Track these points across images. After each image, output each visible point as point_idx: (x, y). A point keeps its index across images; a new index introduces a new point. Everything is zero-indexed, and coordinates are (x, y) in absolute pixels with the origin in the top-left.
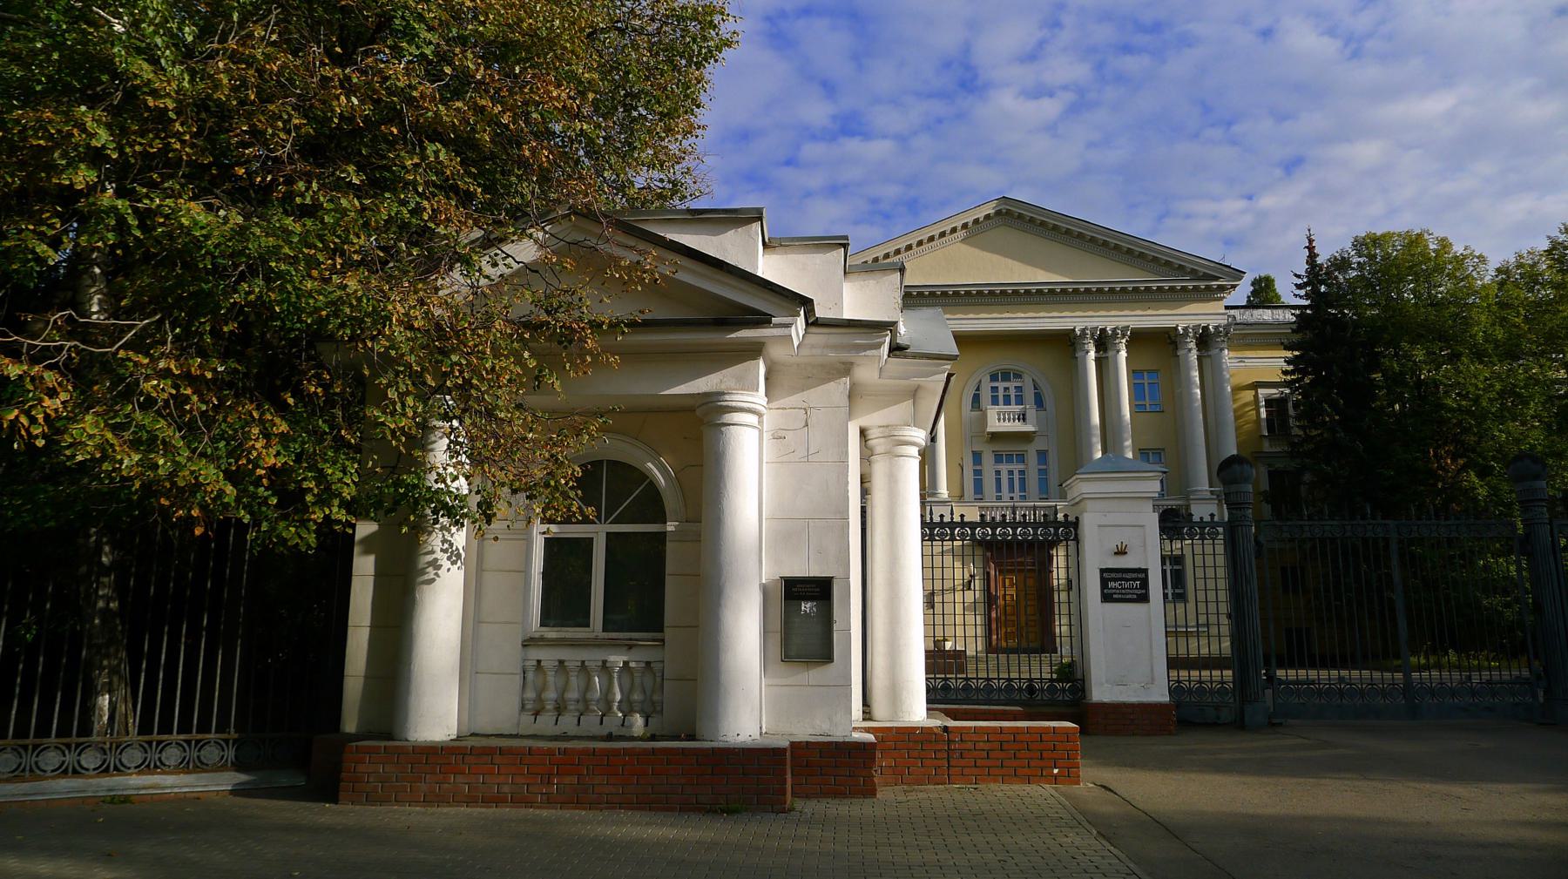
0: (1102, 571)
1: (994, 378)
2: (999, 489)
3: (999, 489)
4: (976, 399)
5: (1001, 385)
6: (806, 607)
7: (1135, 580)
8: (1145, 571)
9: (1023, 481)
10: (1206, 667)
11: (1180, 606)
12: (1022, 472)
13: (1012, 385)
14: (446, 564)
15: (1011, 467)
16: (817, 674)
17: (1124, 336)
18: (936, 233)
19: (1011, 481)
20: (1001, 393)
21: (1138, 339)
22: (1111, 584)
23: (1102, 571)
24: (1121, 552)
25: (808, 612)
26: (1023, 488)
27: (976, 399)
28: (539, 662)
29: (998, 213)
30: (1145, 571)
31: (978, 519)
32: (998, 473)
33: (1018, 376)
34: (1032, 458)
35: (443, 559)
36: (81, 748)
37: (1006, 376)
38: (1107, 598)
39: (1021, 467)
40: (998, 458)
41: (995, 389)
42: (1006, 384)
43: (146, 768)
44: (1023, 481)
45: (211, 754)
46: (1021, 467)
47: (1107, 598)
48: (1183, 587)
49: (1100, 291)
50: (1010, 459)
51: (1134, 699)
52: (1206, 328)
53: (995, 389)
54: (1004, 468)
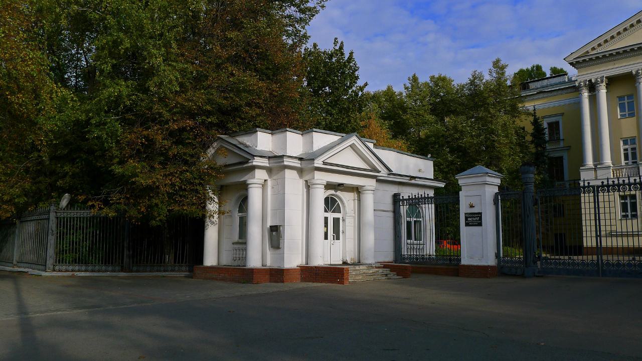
6: (274, 233)
7: (477, 217)
8: (481, 213)
11: (635, 221)
14: (210, 225)
16: (278, 251)
17: (602, 82)
21: (612, 81)
22: (469, 219)
24: (472, 206)
25: (275, 234)
31: (601, 184)
35: (209, 223)
36: (160, 266)
38: (467, 225)
43: (172, 271)
45: (184, 268)
47: (467, 225)
48: (636, 211)
51: (475, 264)
52: (590, 81)
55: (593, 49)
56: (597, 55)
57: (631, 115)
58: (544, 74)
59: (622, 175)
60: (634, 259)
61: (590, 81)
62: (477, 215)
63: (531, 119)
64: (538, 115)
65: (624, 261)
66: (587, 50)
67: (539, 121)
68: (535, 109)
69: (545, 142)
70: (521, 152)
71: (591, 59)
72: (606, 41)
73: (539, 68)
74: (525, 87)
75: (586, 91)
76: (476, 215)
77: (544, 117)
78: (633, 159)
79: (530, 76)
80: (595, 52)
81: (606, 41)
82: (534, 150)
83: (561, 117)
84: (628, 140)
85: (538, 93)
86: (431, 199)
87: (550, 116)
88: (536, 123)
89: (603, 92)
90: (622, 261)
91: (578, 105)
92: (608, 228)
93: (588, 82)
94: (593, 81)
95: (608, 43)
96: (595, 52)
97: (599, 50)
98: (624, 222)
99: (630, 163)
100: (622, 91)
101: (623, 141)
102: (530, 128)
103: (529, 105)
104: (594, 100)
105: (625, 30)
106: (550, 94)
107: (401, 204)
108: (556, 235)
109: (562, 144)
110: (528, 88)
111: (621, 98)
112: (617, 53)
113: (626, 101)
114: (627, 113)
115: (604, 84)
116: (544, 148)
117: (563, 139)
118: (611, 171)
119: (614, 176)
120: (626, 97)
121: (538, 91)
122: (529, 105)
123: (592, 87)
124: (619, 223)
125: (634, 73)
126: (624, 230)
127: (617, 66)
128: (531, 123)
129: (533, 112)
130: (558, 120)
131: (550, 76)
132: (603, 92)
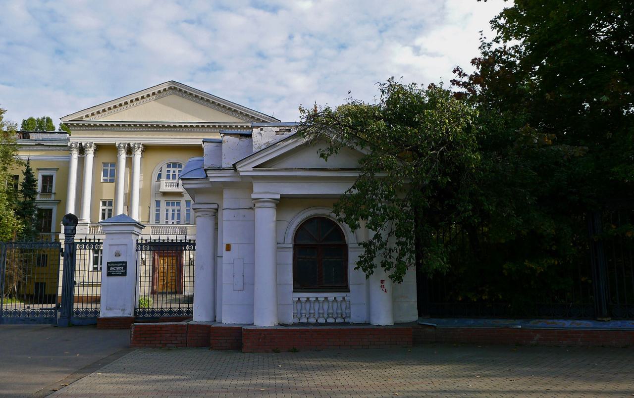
0: (108, 263)
1: (169, 166)
2: (167, 218)
3: (167, 218)
4: (160, 176)
5: (172, 170)
8: (126, 263)
9: (179, 215)
10: (92, 303)
12: (178, 210)
13: (177, 170)
15: (173, 208)
18: (112, 106)
19: (173, 215)
20: (171, 173)
22: (111, 269)
23: (108, 263)
24: (118, 255)
26: (178, 218)
27: (160, 176)
28: (299, 299)
29: (170, 88)
30: (126, 263)
32: (167, 210)
33: (180, 166)
34: (183, 203)
37: (174, 165)
39: (178, 208)
40: (168, 204)
41: (169, 171)
42: (174, 169)
44: (179, 215)
46: (178, 208)
49: (208, 126)
50: (173, 205)
52: (81, 144)
53: (169, 171)
54: (170, 209)
55: (87, 116)
56: (130, 123)
57: (112, 181)
58: (53, 128)
59: (175, 232)
60: (29, 308)
61: (129, 145)
62: (120, 265)
63: (24, 169)
64: (31, 166)
65: (82, 308)
66: (81, 116)
67: (31, 172)
68: (29, 160)
69: (36, 193)
70: (8, 200)
71: (84, 125)
72: (98, 112)
73: (49, 120)
74: (25, 135)
75: (77, 153)
76: (120, 265)
77: (38, 169)
78: (177, 220)
79: (40, 126)
80: (88, 119)
81: (98, 112)
82: (22, 200)
83: (55, 172)
84: (106, 202)
85: (36, 145)
86: (141, 246)
87: (45, 169)
88: (28, 173)
89: (90, 156)
90: (90, 309)
91: (68, 163)
92: (81, 279)
93: (78, 145)
94: (83, 145)
95: (100, 115)
96: (88, 119)
97: (92, 118)
98: (95, 273)
99: (175, 223)
100: (106, 158)
101: (103, 202)
102: (22, 179)
103: (23, 155)
104: (82, 162)
105: (115, 107)
106: (47, 148)
107: (78, 248)
108: (37, 284)
109: (53, 197)
110: (29, 138)
111: (105, 164)
112: (134, 125)
113: (109, 168)
114: (108, 178)
115: (92, 149)
116: (34, 199)
117: (55, 193)
118: (88, 227)
119: (90, 232)
120: (109, 164)
121: (37, 142)
122: (23, 155)
123: (130, 150)
124: (91, 274)
125: (117, 145)
126: (91, 280)
127: (104, 136)
128: (23, 172)
129: (26, 163)
130: (52, 174)
131: (58, 131)
132: (90, 156)
